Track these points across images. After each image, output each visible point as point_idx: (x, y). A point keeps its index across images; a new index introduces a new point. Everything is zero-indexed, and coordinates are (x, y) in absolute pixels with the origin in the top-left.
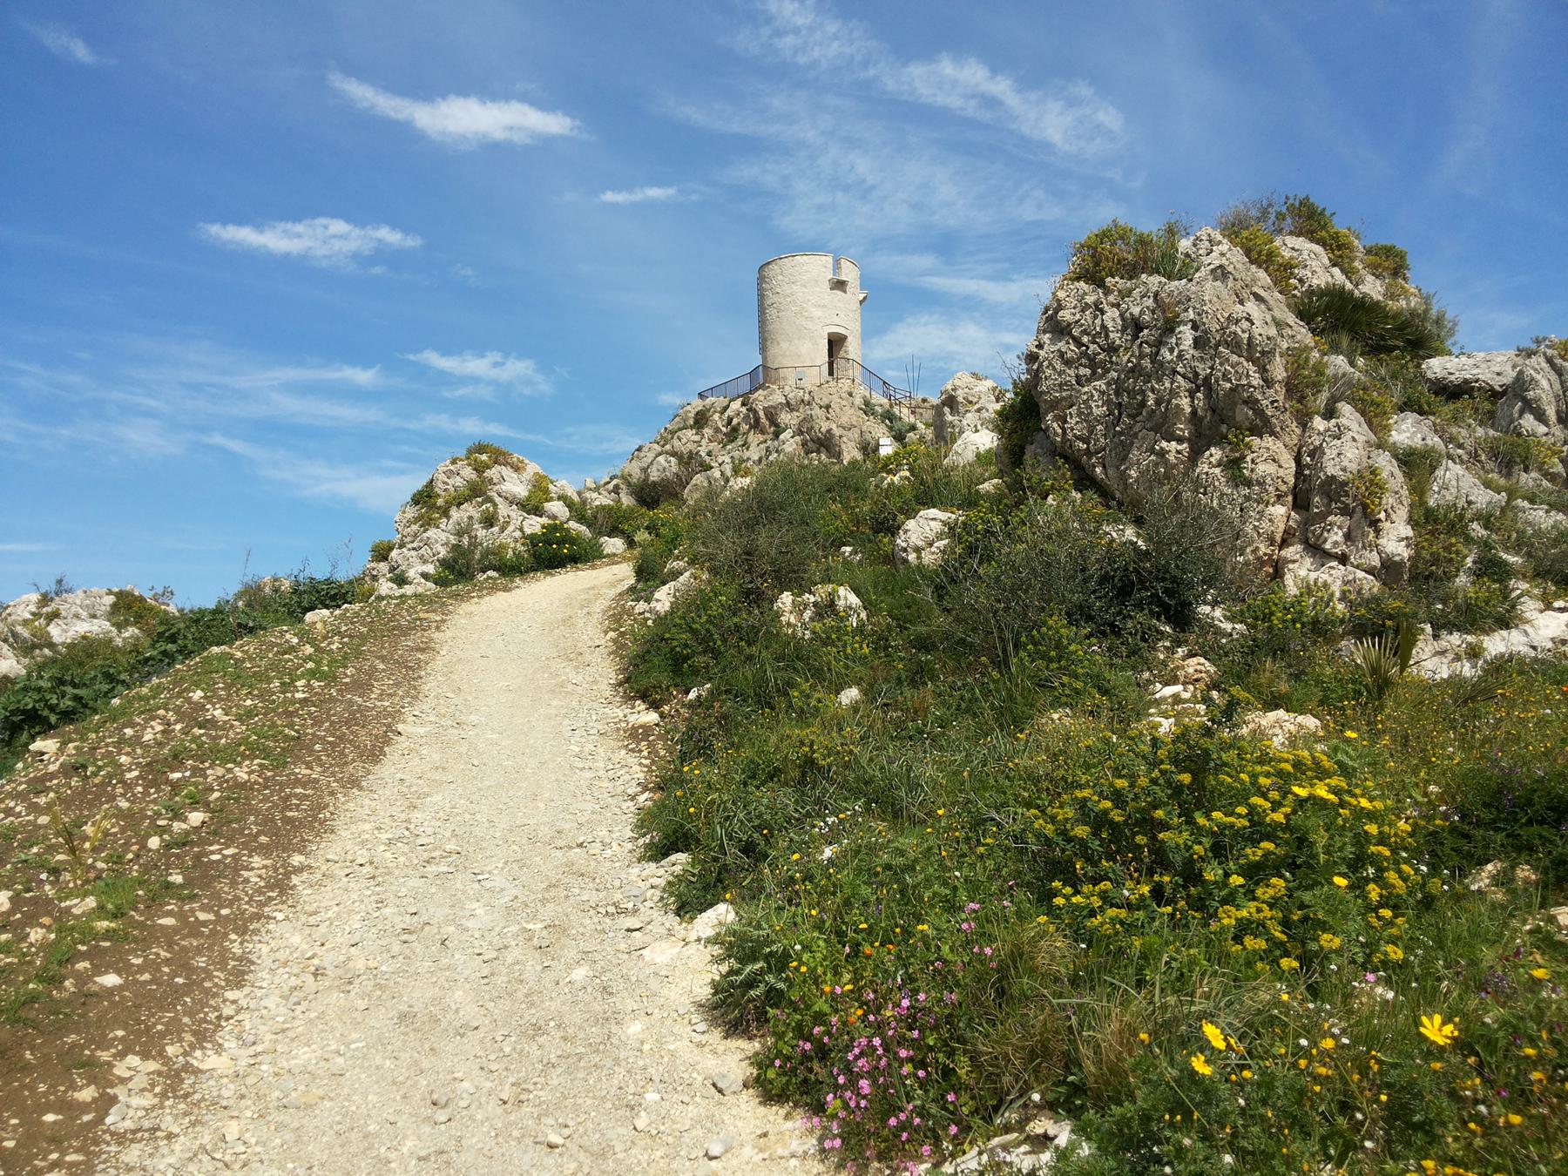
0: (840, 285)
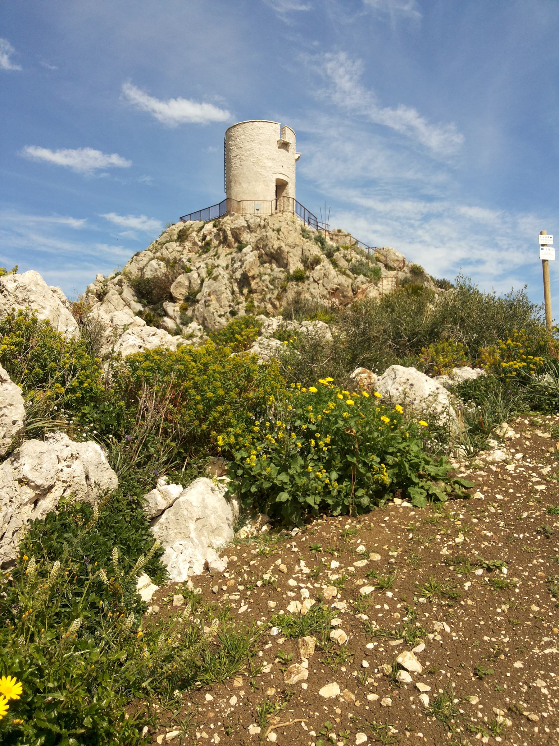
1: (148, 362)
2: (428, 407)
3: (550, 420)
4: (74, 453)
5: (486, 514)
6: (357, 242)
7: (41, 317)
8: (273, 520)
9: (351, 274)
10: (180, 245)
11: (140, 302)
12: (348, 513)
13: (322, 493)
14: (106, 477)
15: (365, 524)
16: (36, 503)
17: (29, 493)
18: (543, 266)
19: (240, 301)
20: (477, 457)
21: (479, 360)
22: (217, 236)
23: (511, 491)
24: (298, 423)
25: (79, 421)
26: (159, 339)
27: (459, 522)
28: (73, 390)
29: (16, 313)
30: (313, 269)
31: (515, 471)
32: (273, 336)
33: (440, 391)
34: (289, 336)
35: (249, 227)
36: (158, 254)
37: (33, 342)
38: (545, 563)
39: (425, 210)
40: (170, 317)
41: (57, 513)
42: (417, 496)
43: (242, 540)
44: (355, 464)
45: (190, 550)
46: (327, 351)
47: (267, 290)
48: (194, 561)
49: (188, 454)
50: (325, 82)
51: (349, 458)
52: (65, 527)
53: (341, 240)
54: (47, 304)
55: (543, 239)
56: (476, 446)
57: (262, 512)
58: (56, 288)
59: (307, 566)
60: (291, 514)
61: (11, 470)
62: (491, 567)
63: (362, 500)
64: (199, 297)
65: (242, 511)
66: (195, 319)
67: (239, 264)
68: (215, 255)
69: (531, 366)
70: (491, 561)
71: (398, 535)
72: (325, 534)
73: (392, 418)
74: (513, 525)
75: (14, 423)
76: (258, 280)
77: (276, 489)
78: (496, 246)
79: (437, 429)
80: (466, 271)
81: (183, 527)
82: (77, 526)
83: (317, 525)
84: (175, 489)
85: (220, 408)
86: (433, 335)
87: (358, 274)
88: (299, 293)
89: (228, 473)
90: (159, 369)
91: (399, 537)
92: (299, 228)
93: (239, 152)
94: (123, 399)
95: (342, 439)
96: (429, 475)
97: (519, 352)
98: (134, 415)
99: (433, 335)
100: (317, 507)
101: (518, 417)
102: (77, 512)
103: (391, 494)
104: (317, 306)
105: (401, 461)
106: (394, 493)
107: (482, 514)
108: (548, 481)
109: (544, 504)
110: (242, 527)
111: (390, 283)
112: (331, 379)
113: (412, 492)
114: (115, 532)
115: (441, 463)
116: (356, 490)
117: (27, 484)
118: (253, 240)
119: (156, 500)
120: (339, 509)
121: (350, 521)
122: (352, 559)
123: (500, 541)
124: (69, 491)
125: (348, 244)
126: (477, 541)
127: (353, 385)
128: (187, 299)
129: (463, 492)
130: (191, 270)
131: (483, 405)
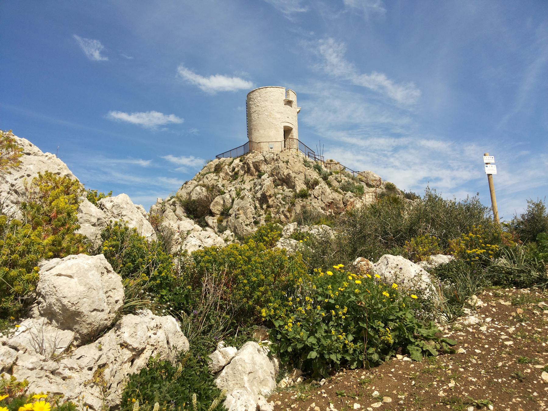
1: (207, 257)
2: (415, 285)
3: (509, 292)
4: (158, 324)
5: (470, 364)
6: (345, 168)
7: (131, 226)
8: (305, 373)
9: (341, 191)
10: (216, 176)
11: (188, 217)
12: (362, 367)
13: (342, 352)
14: (181, 342)
15: (376, 375)
16: (132, 361)
17: (128, 354)
18: (489, 179)
19: (261, 213)
20: (456, 322)
21: (449, 249)
22: (243, 167)
23: (486, 346)
24: (320, 299)
25: (159, 301)
26: (213, 240)
27: (450, 371)
28: (154, 278)
29: (113, 224)
30: (314, 189)
31: (487, 331)
32: (291, 237)
33: (422, 273)
34: (303, 237)
35: (265, 160)
36: (201, 182)
37: (126, 244)
38: (522, 401)
39: (394, 144)
40: (211, 227)
41: (148, 369)
42: (414, 352)
43: (283, 389)
44: (365, 329)
45: (245, 396)
46: (334, 246)
48: (249, 405)
49: (240, 323)
50: (320, 59)
51: (361, 325)
52: (154, 380)
53: (333, 167)
54: (134, 217)
55: (486, 159)
56: (454, 313)
57: (297, 367)
58: (139, 206)
59: (335, 408)
60: (319, 368)
61: (115, 337)
62: (480, 405)
63: (373, 356)
64: (231, 211)
65: (281, 366)
66: (228, 228)
67: (260, 187)
68: (242, 182)
69: (490, 252)
70: (479, 401)
71: (403, 382)
72: (346, 383)
73: (391, 293)
74: (492, 373)
75: (117, 302)
76: (274, 198)
77: (307, 349)
78: (449, 167)
79: (423, 301)
80: (431, 185)
81: (239, 379)
82: (162, 379)
83: (339, 376)
84: (231, 351)
85: (262, 289)
86: (412, 232)
87: (347, 191)
88: (303, 207)
89: (270, 338)
90: (215, 261)
91: (404, 384)
92: (302, 160)
93: (257, 109)
94: (189, 284)
95: (355, 310)
96: (422, 335)
97: (479, 242)
98: (198, 296)
99: (412, 232)
100: (339, 362)
101: (483, 291)
102: (162, 368)
103: (394, 351)
104: (319, 215)
105: (400, 326)
106: (396, 350)
107: (467, 365)
108: (514, 338)
109: (514, 356)
110: (282, 379)
111: (371, 197)
112: (341, 265)
113: (410, 349)
114: (189, 383)
115: (430, 327)
116: (368, 349)
117: (126, 347)
118: (269, 170)
119: (218, 359)
120: (355, 363)
121: (364, 373)
122: (370, 401)
123: (483, 385)
124: (155, 352)
125: (338, 170)
126: (465, 385)
127: (356, 270)
128: (222, 214)
129: (449, 349)
130: (225, 193)
131: (456, 282)
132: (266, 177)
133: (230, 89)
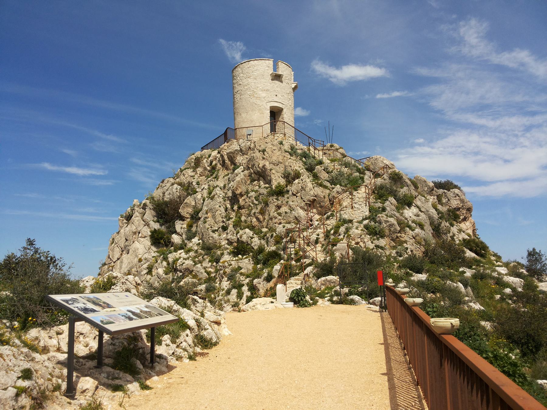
0: (277, 77)
10: (193, 171)
11: (158, 222)
35: (241, 150)
39: (527, 123)
40: (178, 234)
47: (252, 205)
50: (460, 42)
64: (200, 215)
76: (245, 196)
87: (335, 185)
132: (240, 171)
133: (361, 78)
